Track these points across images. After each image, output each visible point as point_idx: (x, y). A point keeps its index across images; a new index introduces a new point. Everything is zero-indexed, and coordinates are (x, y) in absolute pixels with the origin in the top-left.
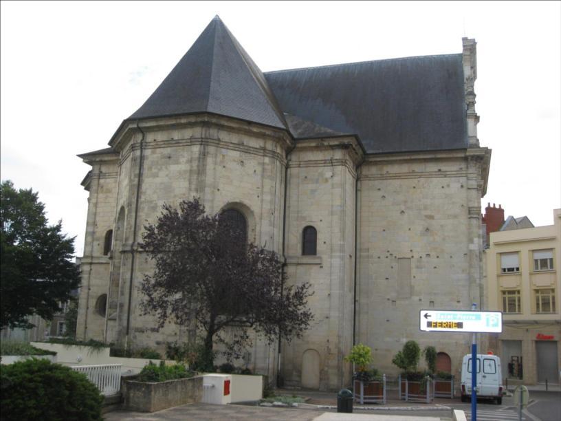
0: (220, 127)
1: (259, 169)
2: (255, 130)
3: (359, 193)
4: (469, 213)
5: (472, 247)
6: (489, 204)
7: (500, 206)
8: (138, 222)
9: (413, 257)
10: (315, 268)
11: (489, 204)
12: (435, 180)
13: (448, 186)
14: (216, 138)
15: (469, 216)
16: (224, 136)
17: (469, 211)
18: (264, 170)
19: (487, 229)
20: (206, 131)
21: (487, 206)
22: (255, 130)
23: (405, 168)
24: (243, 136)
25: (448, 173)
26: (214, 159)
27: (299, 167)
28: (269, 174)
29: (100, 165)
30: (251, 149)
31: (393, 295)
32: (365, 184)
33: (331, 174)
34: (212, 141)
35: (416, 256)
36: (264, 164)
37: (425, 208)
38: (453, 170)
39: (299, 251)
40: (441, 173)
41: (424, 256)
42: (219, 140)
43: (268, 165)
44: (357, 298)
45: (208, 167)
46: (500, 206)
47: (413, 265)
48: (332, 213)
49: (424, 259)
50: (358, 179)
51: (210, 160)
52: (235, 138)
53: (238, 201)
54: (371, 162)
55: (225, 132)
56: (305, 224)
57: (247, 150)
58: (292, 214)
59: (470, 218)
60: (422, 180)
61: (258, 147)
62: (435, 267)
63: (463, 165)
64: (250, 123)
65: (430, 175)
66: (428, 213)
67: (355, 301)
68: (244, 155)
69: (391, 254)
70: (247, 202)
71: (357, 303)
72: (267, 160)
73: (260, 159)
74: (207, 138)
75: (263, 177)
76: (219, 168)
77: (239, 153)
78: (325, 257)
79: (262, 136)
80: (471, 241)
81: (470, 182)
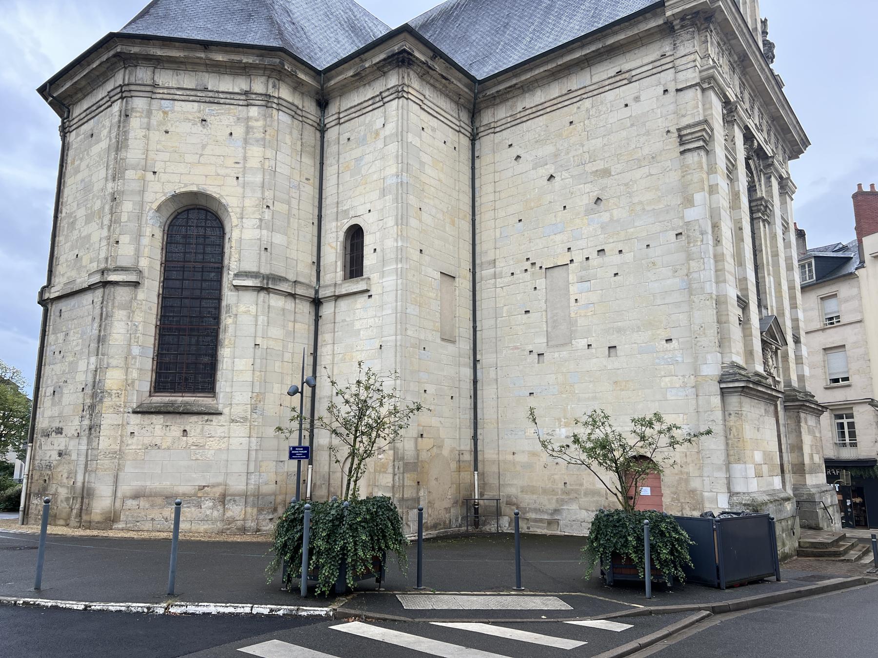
0: (157, 63)
1: (239, 131)
2: (220, 57)
3: (477, 161)
4: (682, 143)
5: (691, 214)
6: (860, 186)
7: (872, 186)
8: (487, 412)
9: (572, 261)
10: (362, 300)
11: (860, 186)
12: (610, 96)
13: (637, 99)
14: (149, 82)
15: (682, 149)
16: (166, 78)
17: (680, 136)
18: (248, 130)
19: (858, 234)
20: (130, 74)
21: (856, 190)
22: (220, 57)
23: (555, 90)
24: (206, 75)
25: (634, 73)
26: (146, 120)
27: (339, 124)
28: (259, 135)
29: (336, 300)
30: (221, 96)
31: (539, 343)
32: (486, 143)
33: (382, 121)
34: (139, 88)
35: (579, 258)
36: (248, 119)
37: (593, 160)
38: (645, 62)
39: (340, 274)
40: (624, 78)
41: (593, 255)
42: (155, 85)
43: (257, 120)
44: (478, 357)
45: (131, 135)
46: (872, 186)
47: (572, 278)
48: (383, 193)
49: (595, 260)
50: (474, 138)
51: (135, 123)
52: (188, 81)
53: (194, 189)
54: (494, 97)
55: (170, 72)
56: (347, 224)
57: (214, 99)
58: (329, 211)
59: (682, 153)
60: (587, 103)
61: (237, 90)
62: (616, 274)
63: (667, 47)
64: (206, 45)
65: (600, 89)
66: (600, 165)
67: (475, 361)
68: (207, 109)
69: (533, 264)
70: (212, 190)
71: (478, 366)
72: (254, 111)
73: (242, 111)
74: (128, 85)
75: (246, 141)
76: (156, 136)
77: (196, 104)
78: (375, 277)
79: (244, 70)
80: (689, 202)
81: (681, 76)
